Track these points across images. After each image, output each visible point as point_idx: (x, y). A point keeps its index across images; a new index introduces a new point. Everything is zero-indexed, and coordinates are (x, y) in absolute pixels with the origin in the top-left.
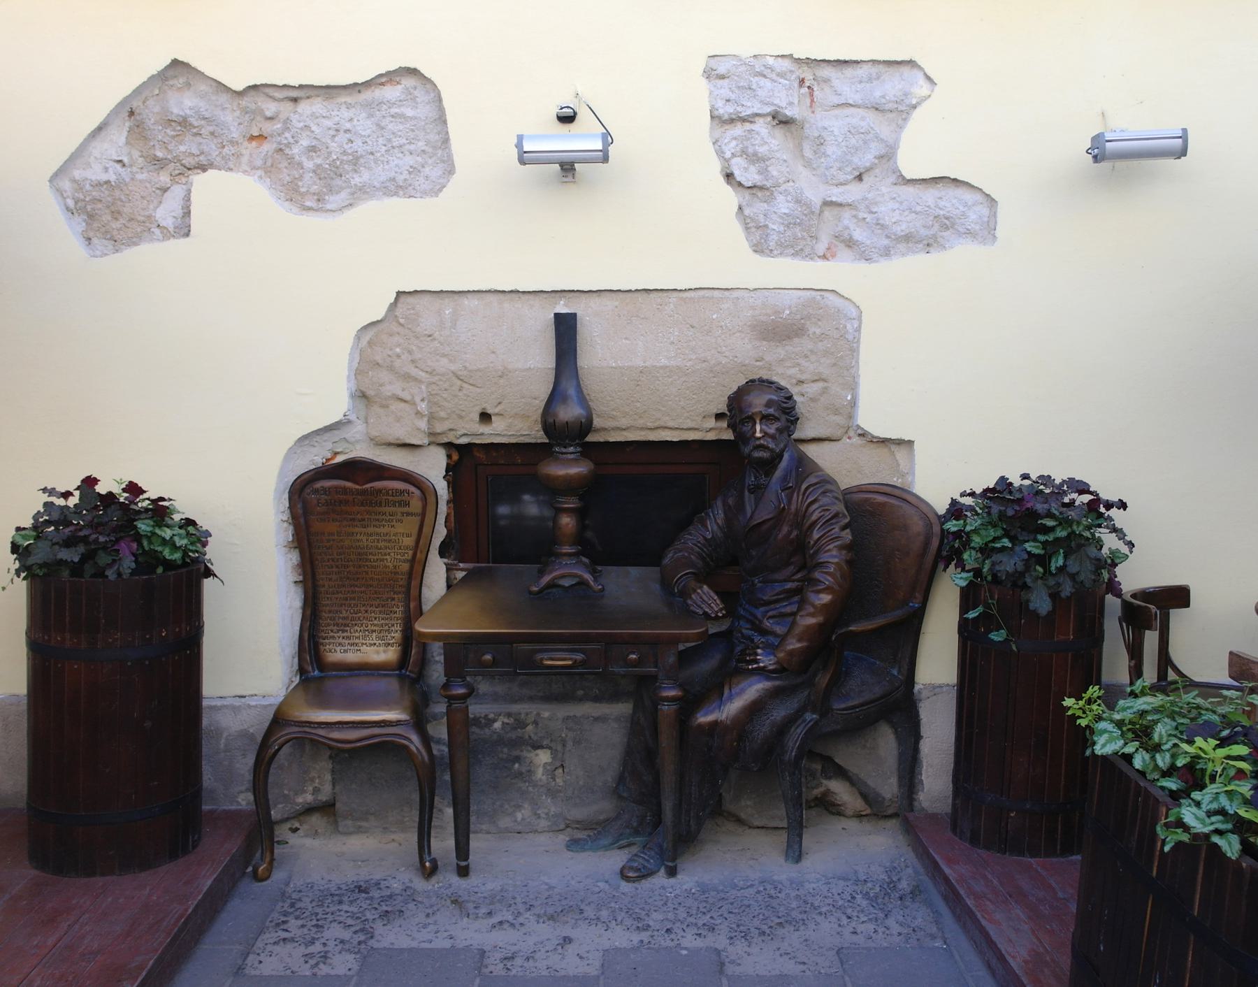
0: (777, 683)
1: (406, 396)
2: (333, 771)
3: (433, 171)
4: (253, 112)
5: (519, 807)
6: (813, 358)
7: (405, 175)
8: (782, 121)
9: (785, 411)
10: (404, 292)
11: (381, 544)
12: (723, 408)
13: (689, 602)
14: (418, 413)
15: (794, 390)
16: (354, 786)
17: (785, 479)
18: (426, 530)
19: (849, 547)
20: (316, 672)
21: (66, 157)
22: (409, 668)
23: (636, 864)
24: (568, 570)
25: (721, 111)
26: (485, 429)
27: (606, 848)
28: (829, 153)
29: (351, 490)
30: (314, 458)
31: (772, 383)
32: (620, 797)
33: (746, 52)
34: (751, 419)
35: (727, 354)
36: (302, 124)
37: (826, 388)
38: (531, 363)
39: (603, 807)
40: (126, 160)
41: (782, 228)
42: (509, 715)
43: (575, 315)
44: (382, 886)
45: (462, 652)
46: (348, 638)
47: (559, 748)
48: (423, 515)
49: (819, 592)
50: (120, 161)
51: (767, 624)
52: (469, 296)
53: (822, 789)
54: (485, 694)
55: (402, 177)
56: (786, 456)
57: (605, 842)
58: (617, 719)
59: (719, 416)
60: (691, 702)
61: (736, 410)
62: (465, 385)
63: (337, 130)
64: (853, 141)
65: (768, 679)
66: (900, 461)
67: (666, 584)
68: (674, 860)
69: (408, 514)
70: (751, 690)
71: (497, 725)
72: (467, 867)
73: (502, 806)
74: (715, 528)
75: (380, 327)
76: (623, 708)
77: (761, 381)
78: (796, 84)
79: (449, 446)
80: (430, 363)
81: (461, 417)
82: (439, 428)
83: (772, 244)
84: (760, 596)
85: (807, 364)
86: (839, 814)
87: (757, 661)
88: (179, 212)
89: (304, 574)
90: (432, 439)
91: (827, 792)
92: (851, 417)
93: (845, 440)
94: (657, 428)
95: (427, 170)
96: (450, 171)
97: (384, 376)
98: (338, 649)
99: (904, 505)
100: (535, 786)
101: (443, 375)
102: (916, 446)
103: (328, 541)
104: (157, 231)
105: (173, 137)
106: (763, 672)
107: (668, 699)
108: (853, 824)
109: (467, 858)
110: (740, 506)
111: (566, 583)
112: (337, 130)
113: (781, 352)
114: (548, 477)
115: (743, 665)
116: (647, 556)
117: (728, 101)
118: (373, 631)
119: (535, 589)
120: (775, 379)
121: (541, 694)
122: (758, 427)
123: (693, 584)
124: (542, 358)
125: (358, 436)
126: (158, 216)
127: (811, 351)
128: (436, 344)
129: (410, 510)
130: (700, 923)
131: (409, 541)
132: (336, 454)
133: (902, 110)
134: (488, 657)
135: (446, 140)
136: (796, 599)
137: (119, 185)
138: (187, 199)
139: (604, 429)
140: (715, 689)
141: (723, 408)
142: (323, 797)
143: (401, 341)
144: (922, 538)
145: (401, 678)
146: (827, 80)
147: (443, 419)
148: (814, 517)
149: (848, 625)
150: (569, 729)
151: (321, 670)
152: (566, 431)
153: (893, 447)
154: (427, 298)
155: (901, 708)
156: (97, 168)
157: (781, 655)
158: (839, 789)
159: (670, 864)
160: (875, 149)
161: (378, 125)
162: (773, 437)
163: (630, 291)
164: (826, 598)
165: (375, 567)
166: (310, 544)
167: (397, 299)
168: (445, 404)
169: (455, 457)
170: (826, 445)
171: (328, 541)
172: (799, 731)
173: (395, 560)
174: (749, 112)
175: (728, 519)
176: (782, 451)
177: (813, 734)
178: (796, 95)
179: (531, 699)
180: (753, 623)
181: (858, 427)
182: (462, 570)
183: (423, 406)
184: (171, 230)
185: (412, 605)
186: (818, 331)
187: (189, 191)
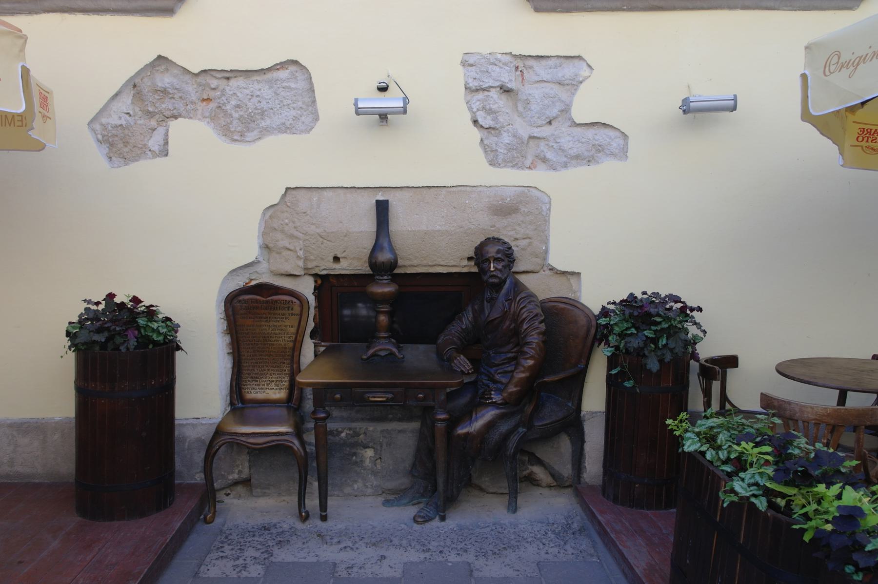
0: (503, 411)
2: (250, 461)
4: (204, 85)
5: (356, 481)
7: (291, 121)
8: (506, 90)
9: (507, 256)
11: (277, 332)
12: (472, 254)
14: (298, 257)
15: (512, 244)
17: (507, 294)
19: (544, 333)
22: (293, 401)
24: (384, 346)
25: (471, 85)
27: (405, 505)
30: (239, 283)
33: (485, 51)
34: (488, 260)
39: (403, 481)
40: (131, 113)
42: (350, 429)
47: (379, 448)
48: (301, 315)
49: (527, 359)
51: (497, 377)
53: (528, 471)
56: (508, 281)
57: (404, 501)
59: (470, 259)
60: (453, 422)
61: (480, 255)
64: (546, 102)
65: (498, 408)
67: (439, 354)
68: (444, 512)
70: (488, 415)
71: (343, 435)
72: (326, 516)
75: (276, 208)
76: (416, 425)
77: (494, 238)
78: (514, 69)
79: (316, 275)
81: (322, 259)
82: (310, 265)
86: (538, 485)
87: (491, 398)
88: (162, 142)
89: (233, 348)
91: (532, 473)
92: (545, 259)
93: (542, 272)
95: (303, 118)
96: (316, 119)
97: (279, 236)
100: (365, 469)
104: (149, 153)
106: (495, 405)
108: (546, 492)
109: (326, 511)
110: (482, 310)
111: (383, 353)
114: (372, 293)
120: (501, 237)
122: (492, 265)
123: (455, 354)
124: (368, 225)
128: (308, 217)
130: (459, 547)
131: (293, 330)
132: (251, 280)
133: (574, 84)
134: (338, 396)
135: (314, 102)
137: (128, 127)
140: (468, 414)
141: (472, 254)
142: (244, 476)
145: (288, 408)
146: (531, 67)
148: (524, 316)
150: (384, 437)
151: (243, 404)
152: (382, 268)
153: (569, 276)
155: (573, 425)
156: (115, 117)
157: (505, 395)
158: (538, 472)
160: (559, 106)
162: (500, 270)
164: (530, 362)
166: (236, 332)
169: (319, 282)
170: (531, 275)
175: (474, 317)
179: (363, 420)
183: (301, 253)
186: (526, 210)
187: (167, 131)
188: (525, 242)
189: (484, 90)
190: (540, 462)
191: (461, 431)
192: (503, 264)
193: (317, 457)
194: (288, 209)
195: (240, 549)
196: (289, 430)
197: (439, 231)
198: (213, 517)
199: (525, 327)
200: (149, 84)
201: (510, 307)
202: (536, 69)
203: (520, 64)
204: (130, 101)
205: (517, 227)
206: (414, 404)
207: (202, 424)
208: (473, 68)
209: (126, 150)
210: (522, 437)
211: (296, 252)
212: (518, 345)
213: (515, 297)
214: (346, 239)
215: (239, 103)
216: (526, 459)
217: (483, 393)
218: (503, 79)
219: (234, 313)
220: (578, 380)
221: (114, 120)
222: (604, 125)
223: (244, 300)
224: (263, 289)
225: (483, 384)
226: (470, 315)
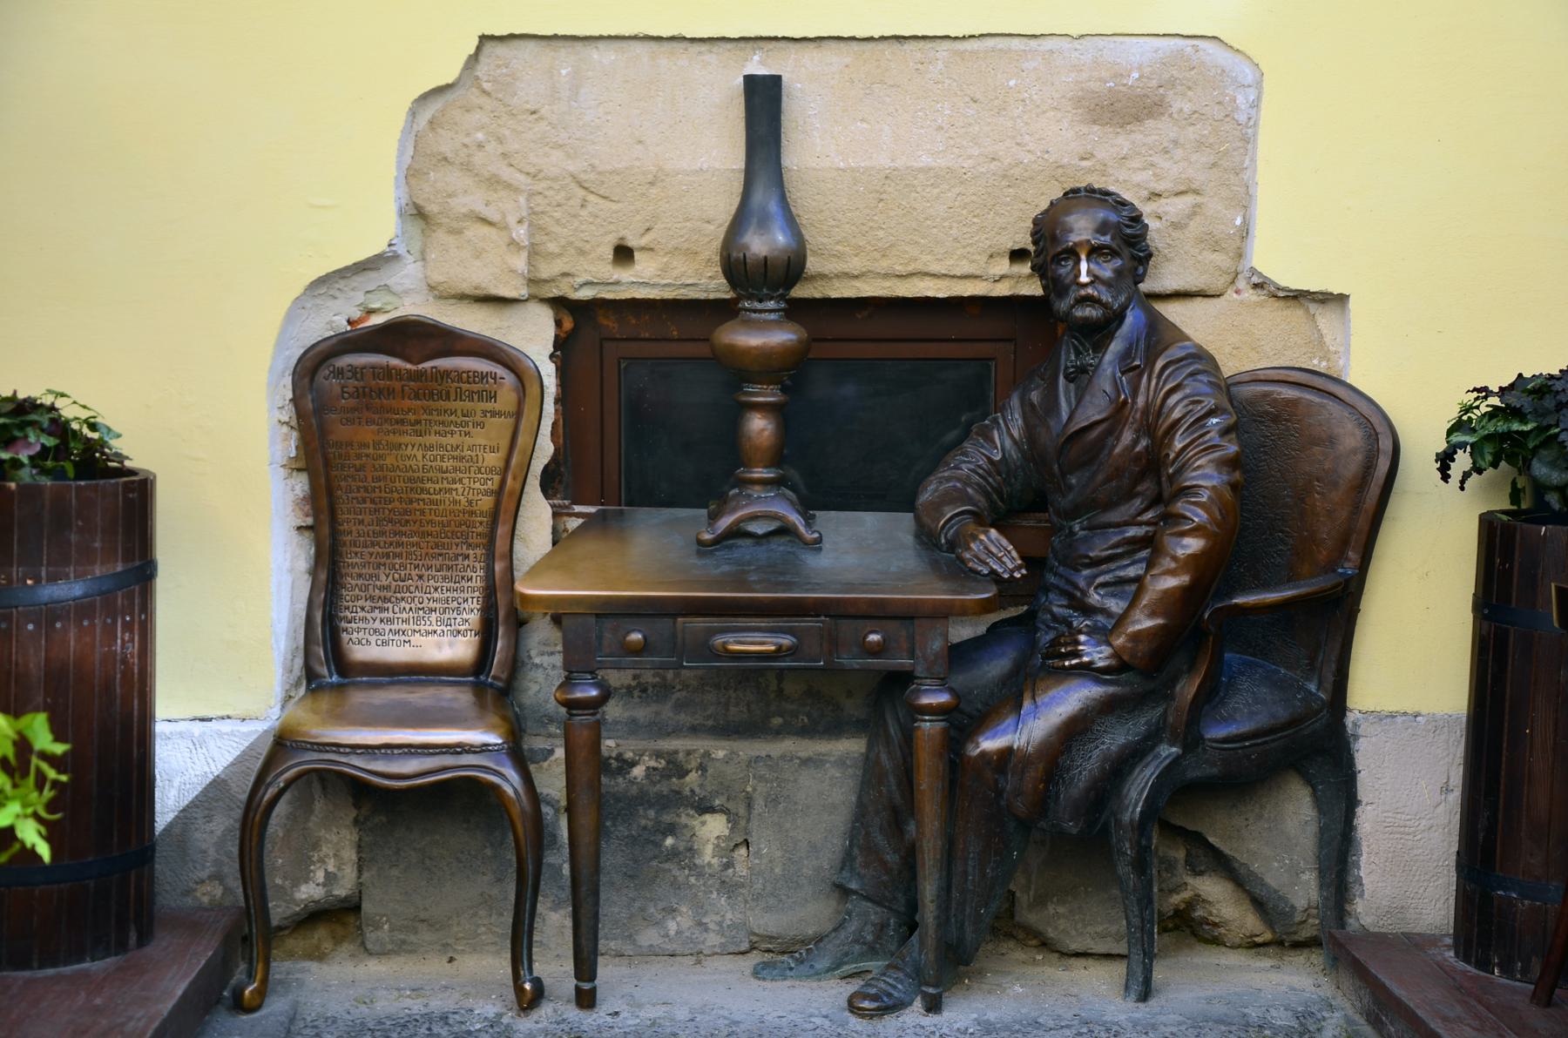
0: (1111, 689)
1: (491, 213)
2: (359, 848)
5: (671, 911)
6: (1179, 153)
9: (1128, 241)
10: (492, 38)
12: (1024, 240)
13: (967, 555)
14: (513, 243)
15: (1146, 209)
16: (395, 872)
17: (1126, 355)
18: (522, 440)
19: (1232, 463)
20: (335, 678)
22: (490, 681)
23: (873, 991)
24: (763, 506)
26: (625, 275)
27: (817, 975)
29: (399, 371)
30: (333, 318)
31: (1108, 194)
32: (843, 892)
34: (1072, 253)
35: (1031, 147)
37: (1198, 205)
39: (810, 913)
42: (658, 755)
43: (779, 77)
44: (451, 1021)
45: (589, 629)
46: (390, 621)
47: (742, 811)
48: (518, 415)
49: (1183, 534)
51: (1095, 598)
52: (601, 45)
53: (1186, 895)
54: (616, 722)
56: (1130, 319)
58: (841, 762)
59: (1017, 255)
60: (964, 721)
61: (1046, 246)
62: (591, 198)
66: (1324, 332)
67: (926, 538)
69: (494, 414)
70: (1064, 702)
71: (638, 772)
72: (593, 991)
73: (643, 909)
74: (1008, 443)
75: (449, 96)
76: (852, 746)
77: (1091, 190)
79: (559, 304)
81: (582, 252)
82: (546, 270)
84: (1082, 551)
85: (1167, 165)
86: (1216, 941)
87: (1077, 654)
89: (316, 513)
90: (534, 290)
91: (1196, 900)
92: (1240, 255)
93: (1230, 295)
94: (911, 275)
98: (373, 639)
99: (1331, 405)
100: (700, 875)
101: (555, 179)
102: (1352, 303)
103: (359, 457)
107: (930, 710)
111: (759, 528)
113: (1122, 142)
114: (732, 350)
115: (1057, 663)
116: (888, 494)
118: (432, 610)
119: (707, 537)
120: (1112, 188)
121: (710, 723)
122: (1084, 266)
123: (972, 528)
124: (722, 151)
125: (408, 283)
127: (1175, 142)
128: (543, 126)
129: (497, 406)
131: (493, 459)
132: (371, 312)
134: (636, 637)
136: (1144, 554)
139: (823, 276)
140: (1010, 697)
141: (1024, 240)
142: (342, 891)
143: (485, 120)
144: (1360, 457)
145: (479, 689)
148: (1176, 414)
149: (1231, 596)
150: (761, 778)
152: (762, 279)
153: (1313, 307)
154: (531, 45)
155: (1320, 750)
157: (1120, 641)
158: (1215, 893)
159: (931, 990)
162: (1108, 284)
163: (871, 39)
164: (1193, 545)
165: (432, 502)
167: (479, 49)
169: (568, 324)
170: (1198, 305)
172: (1148, 772)
173: (474, 492)
175: (1029, 428)
176: (1124, 308)
177: (1179, 791)
179: (694, 730)
180: (1071, 596)
181: (1253, 271)
182: (578, 515)
183: (520, 233)
185: (499, 567)
186: (1187, 107)
188: (1175, 207)
190: (1224, 865)
191: (989, 744)
192: (1118, 262)
193: (570, 809)
194: (483, 100)
196: (493, 739)
198: (262, 993)
199: (1178, 445)
201: (1135, 392)
205: (1156, 159)
206: (856, 663)
207: (220, 735)
210: (1168, 768)
211: (506, 228)
212: (1157, 500)
213: (1150, 361)
214: (654, 191)
216: (1180, 854)
217: (1055, 643)
220: (1332, 615)
223: (355, 371)
224: (408, 336)
225: (1055, 618)
226: (1015, 422)
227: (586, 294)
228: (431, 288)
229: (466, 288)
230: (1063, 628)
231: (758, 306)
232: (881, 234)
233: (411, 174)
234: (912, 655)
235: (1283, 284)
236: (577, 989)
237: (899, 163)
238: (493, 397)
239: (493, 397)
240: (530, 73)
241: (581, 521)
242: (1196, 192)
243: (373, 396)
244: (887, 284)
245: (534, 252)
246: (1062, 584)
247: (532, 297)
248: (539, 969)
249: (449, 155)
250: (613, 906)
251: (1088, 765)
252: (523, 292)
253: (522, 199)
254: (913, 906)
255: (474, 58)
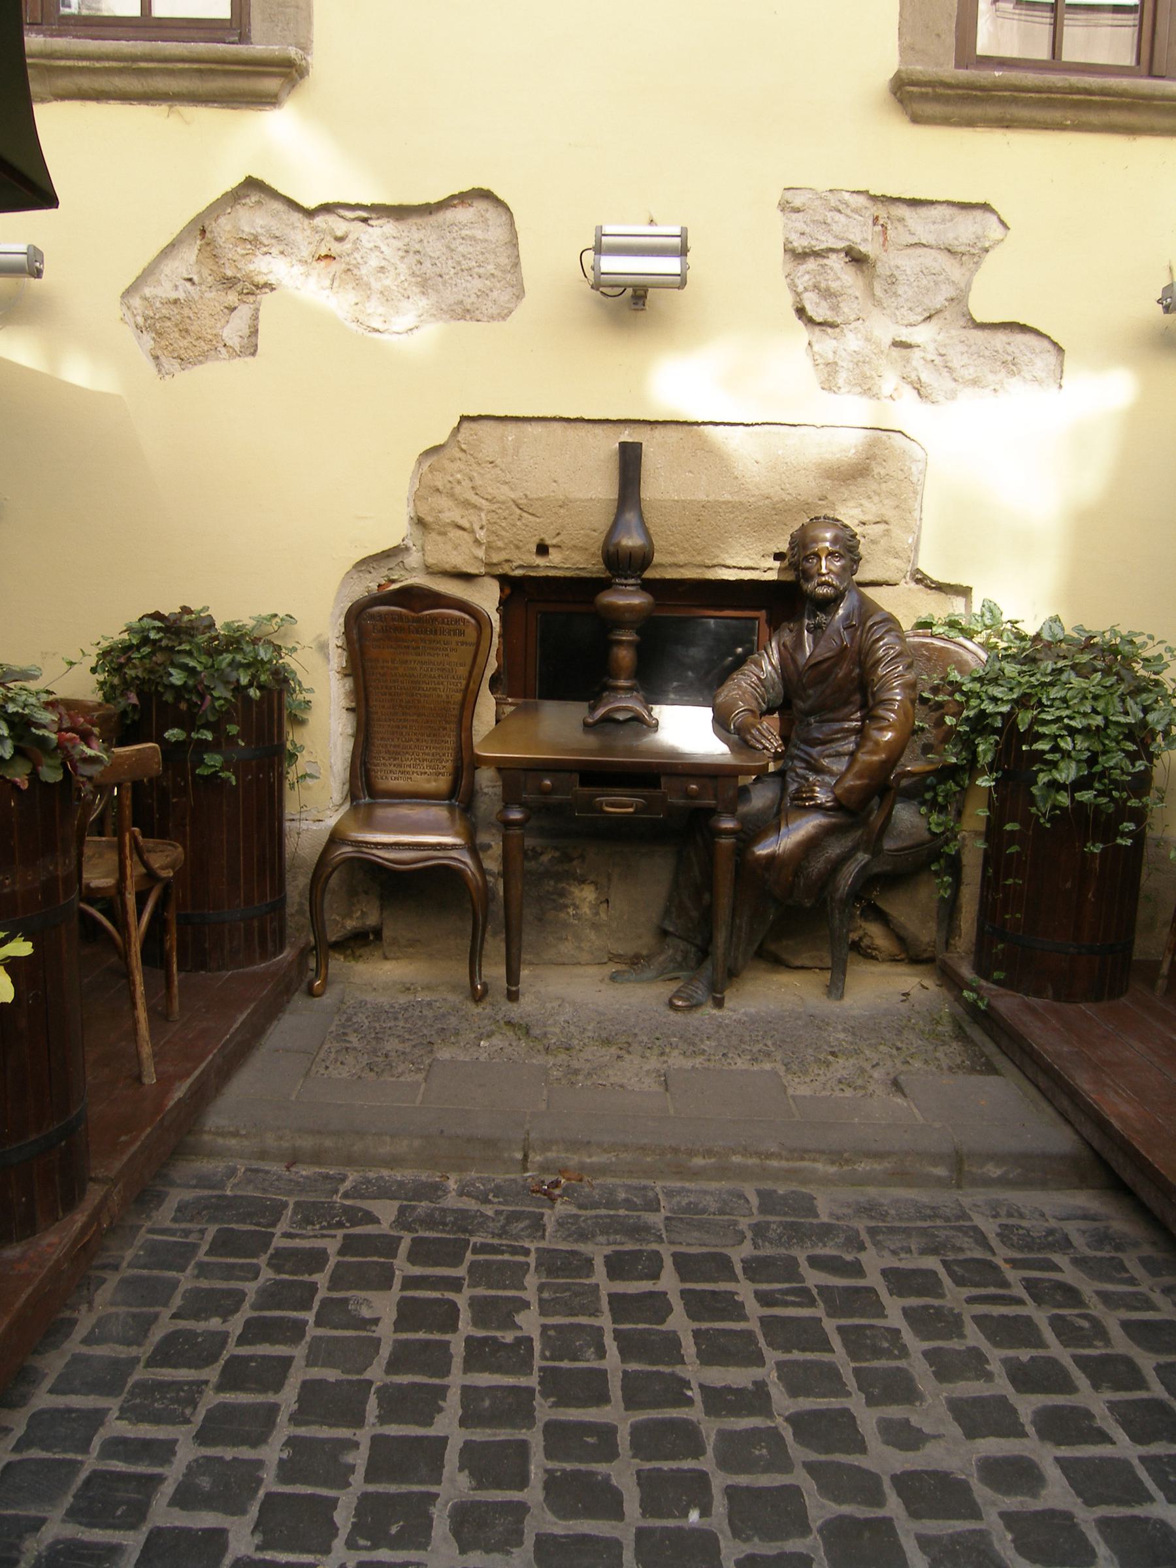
0: (833, 820)
3: (503, 296)
4: (324, 232)
6: (876, 499)
7: (473, 298)
8: (856, 259)
9: (848, 549)
11: (437, 673)
13: (749, 737)
14: (477, 542)
18: (480, 659)
21: (138, 272)
25: (795, 244)
26: (540, 561)
27: (650, 980)
28: (900, 292)
29: (407, 617)
30: (370, 584)
31: (838, 520)
33: (822, 186)
35: (790, 491)
36: (371, 245)
38: (592, 494)
39: (644, 942)
40: (196, 278)
41: (851, 366)
49: (881, 729)
50: (190, 280)
51: (825, 762)
55: (470, 301)
57: (649, 974)
59: (778, 556)
62: (525, 515)
63: (407, 252)
64: (925, 282)
65: (825, 815)
68: (721, 993)
69: (463, 643)
72: (517, 993)
78: (871, 222)
79: (505, 580)
80: (490, 490)
81: (518, 547)
83: (841, 382)
88: (246, 332)
89: (358, 701)
90: (489, 570)
94: (714, 566)
95: (495, 294)
96: (520, 294)
97: (444, 502)
99: (961, 651)
101: (503, 503)
104: (223, 350)
105: (243, 256)
106: (819, 808)
108: (884, 968)
109: (517, 984)
110: (799, 643)
111: (621, 716)
112: (407, 252)
115: (800, 803)
117: (803, 234)
119: (590, 720)
122: (823, 563)
124: (601, 487)
126: (224, 335)
130: (755, 1049)
131: (463, 671)
133: (971, 255)
135: (516, 264)
137: (189, 302)
138: (255, 317)
139: (661, 565)
140: (771, 822)
141: (784, 547)
143: (463, 467)
146: (901, 220)
147: (500, 549)
151: (371, 796)
152: (623, 564)
156: (168, 285)
158: (876, 934)
160: (947, 291)
161: (448, 247)
164: (889, 735)
166: (364, 671)
168: (504, 533)
169: (508, 591)
170: (885, 589)
171: (383, 668)
174: (823, 246)
178: (870, 232)
182: (511, 704)
183: (481, 535)
184: (238, 349)
187: (257, 310)
188: (874, 530)
189: (817, 254)
190: (882, 918)
191: (763, 850)
194: (461, 455)
195: (376, 1038)
197: (726, 503)
200: (228, 228)
202: (910, 222)
203: (881, 211)
204: (194, 257)
208: (800, 216)
209: (185, 343)
211: (473, 532)
214: (562, 511)
215: (383, 263)
217: (798, 791)
218: (851, 237)
219: (362, 634)
221: (164, 289)
222: (1023, 328)
224: (411, 597)
225: (797, 775)
227: (519, 573)
228: (427, 567)
229: (448, 567)
230: (803, 781)
231: (625, 582)
232: (698, 541)
233: (417, 498)
234: (716, 797)
235: (935, 579)
236: (508, 989)
237: (711, 498)
238: (462, 633)
239: (462, 633)
240: (489, 437)
241: (513, 708)
242: (886, 523)
243: (393, 631)
244: (699, 571)
245: (490, 547)
246: (802, 755)
247: (487, 574)
248: (486, 971)
249: (441, 488)
250: (529, 936)
251: (818, 865)
252: (483, 570)
253: (483, 515)
254: (709, 940)
255: (457, 429)
